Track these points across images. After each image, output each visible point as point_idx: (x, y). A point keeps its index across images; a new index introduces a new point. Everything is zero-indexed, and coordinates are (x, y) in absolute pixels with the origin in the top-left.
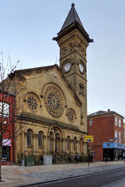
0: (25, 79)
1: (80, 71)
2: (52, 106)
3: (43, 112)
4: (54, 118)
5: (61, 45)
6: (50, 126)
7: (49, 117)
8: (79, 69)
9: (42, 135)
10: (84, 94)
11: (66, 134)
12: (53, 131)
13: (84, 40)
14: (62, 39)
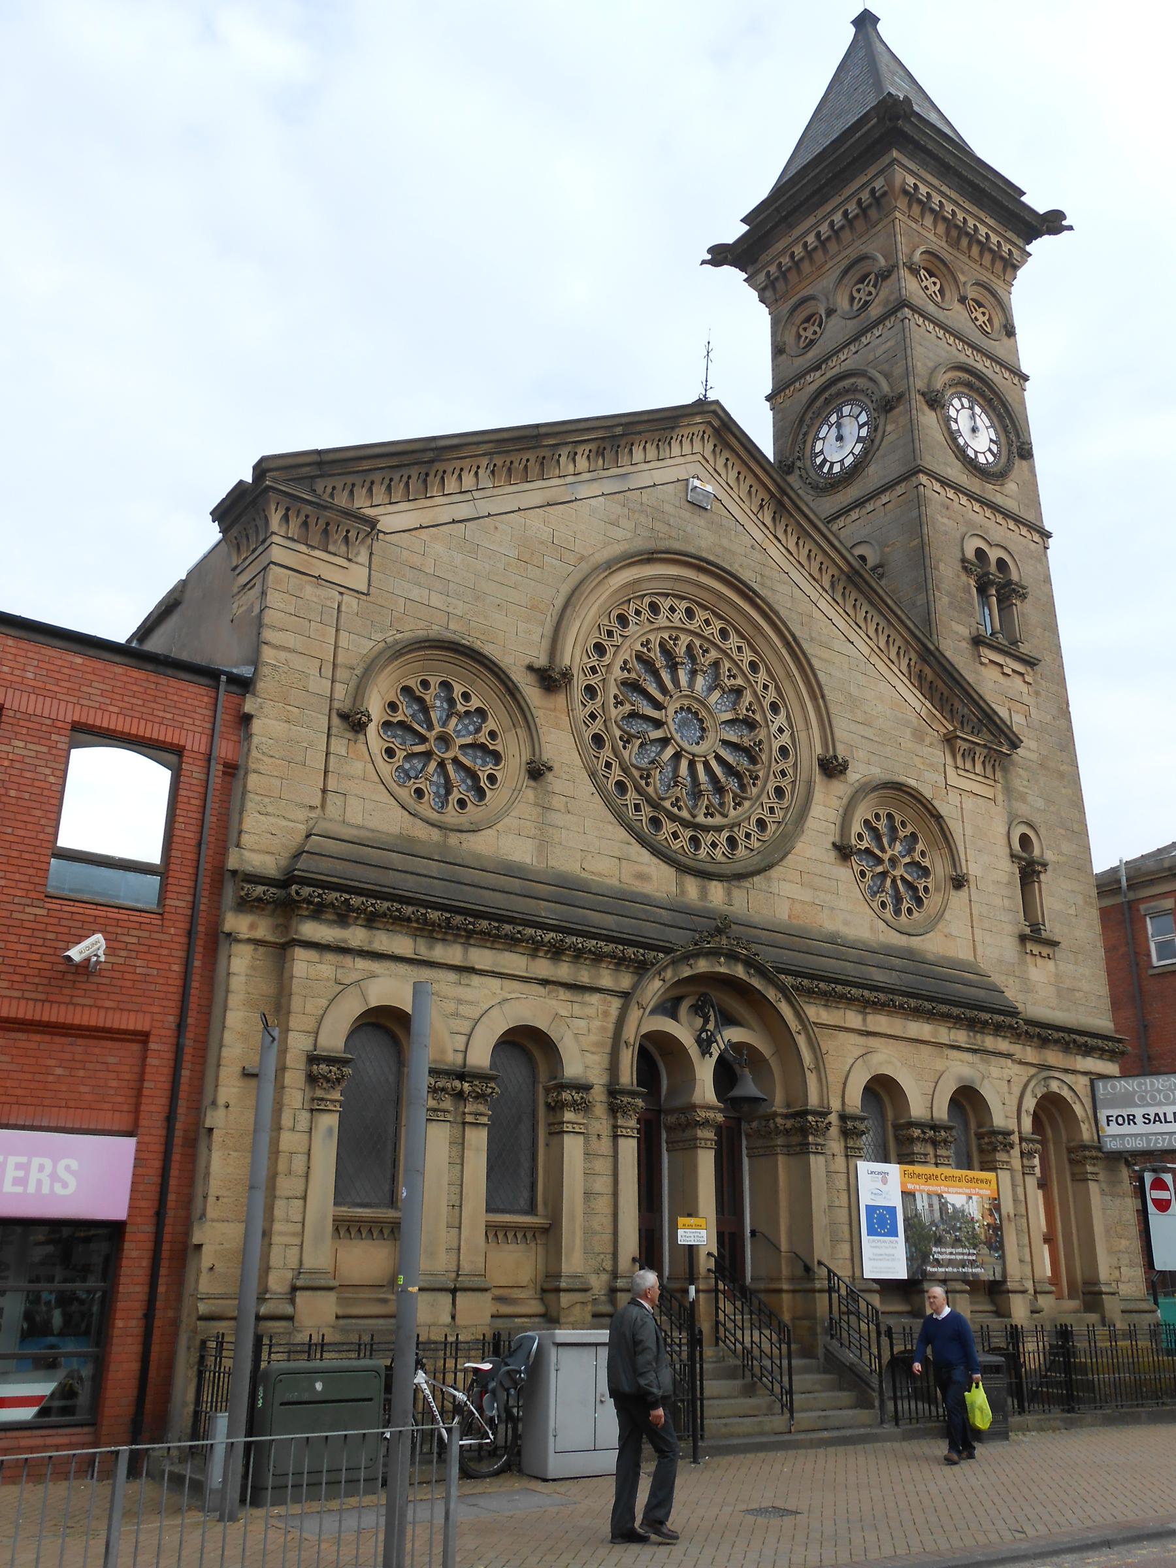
0: (372, 523)
1: (961, 453)
2: (676, 769)
3: (564, 830)
4: (692, 887)
5: (780, 285)
6: (641, 968)
7: (641, 876)
8: (953, 436)
9: (543, 1077)
10: (1024, 648)
11: (848, 1055)
12: (683, 1031)
13: (985, 228)
14: (780, 245)
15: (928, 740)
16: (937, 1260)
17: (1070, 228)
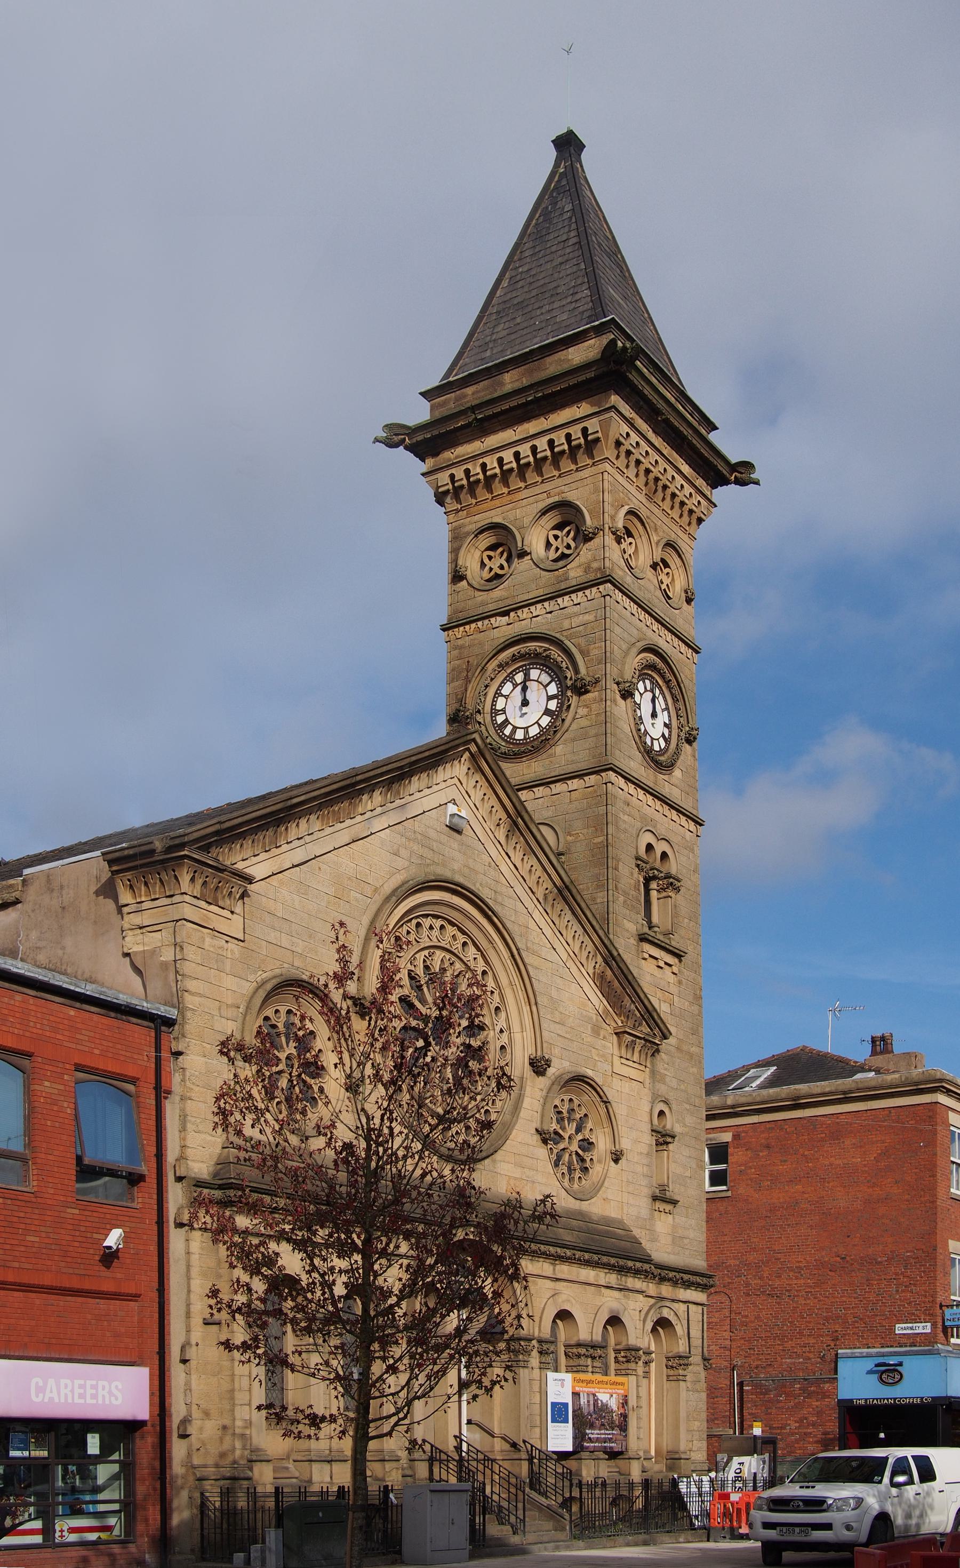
1: (640, 735)
13: (678, 473)
15: (602, 1033)
16: (590, 1438)
17: (757, 483)
